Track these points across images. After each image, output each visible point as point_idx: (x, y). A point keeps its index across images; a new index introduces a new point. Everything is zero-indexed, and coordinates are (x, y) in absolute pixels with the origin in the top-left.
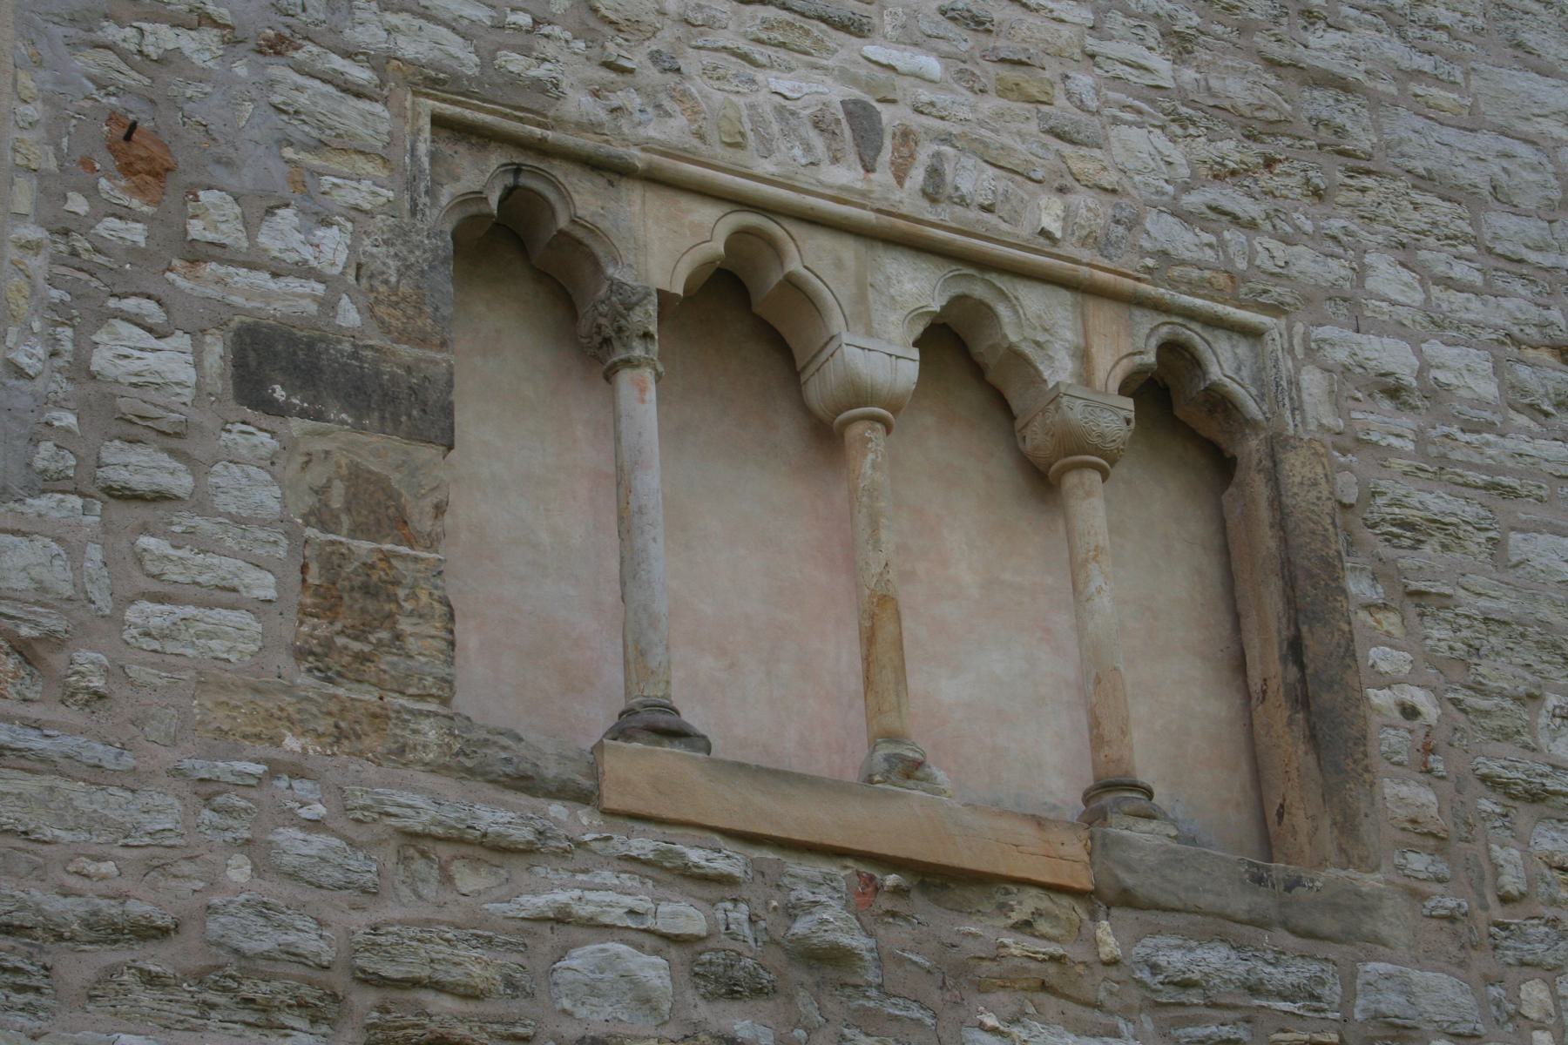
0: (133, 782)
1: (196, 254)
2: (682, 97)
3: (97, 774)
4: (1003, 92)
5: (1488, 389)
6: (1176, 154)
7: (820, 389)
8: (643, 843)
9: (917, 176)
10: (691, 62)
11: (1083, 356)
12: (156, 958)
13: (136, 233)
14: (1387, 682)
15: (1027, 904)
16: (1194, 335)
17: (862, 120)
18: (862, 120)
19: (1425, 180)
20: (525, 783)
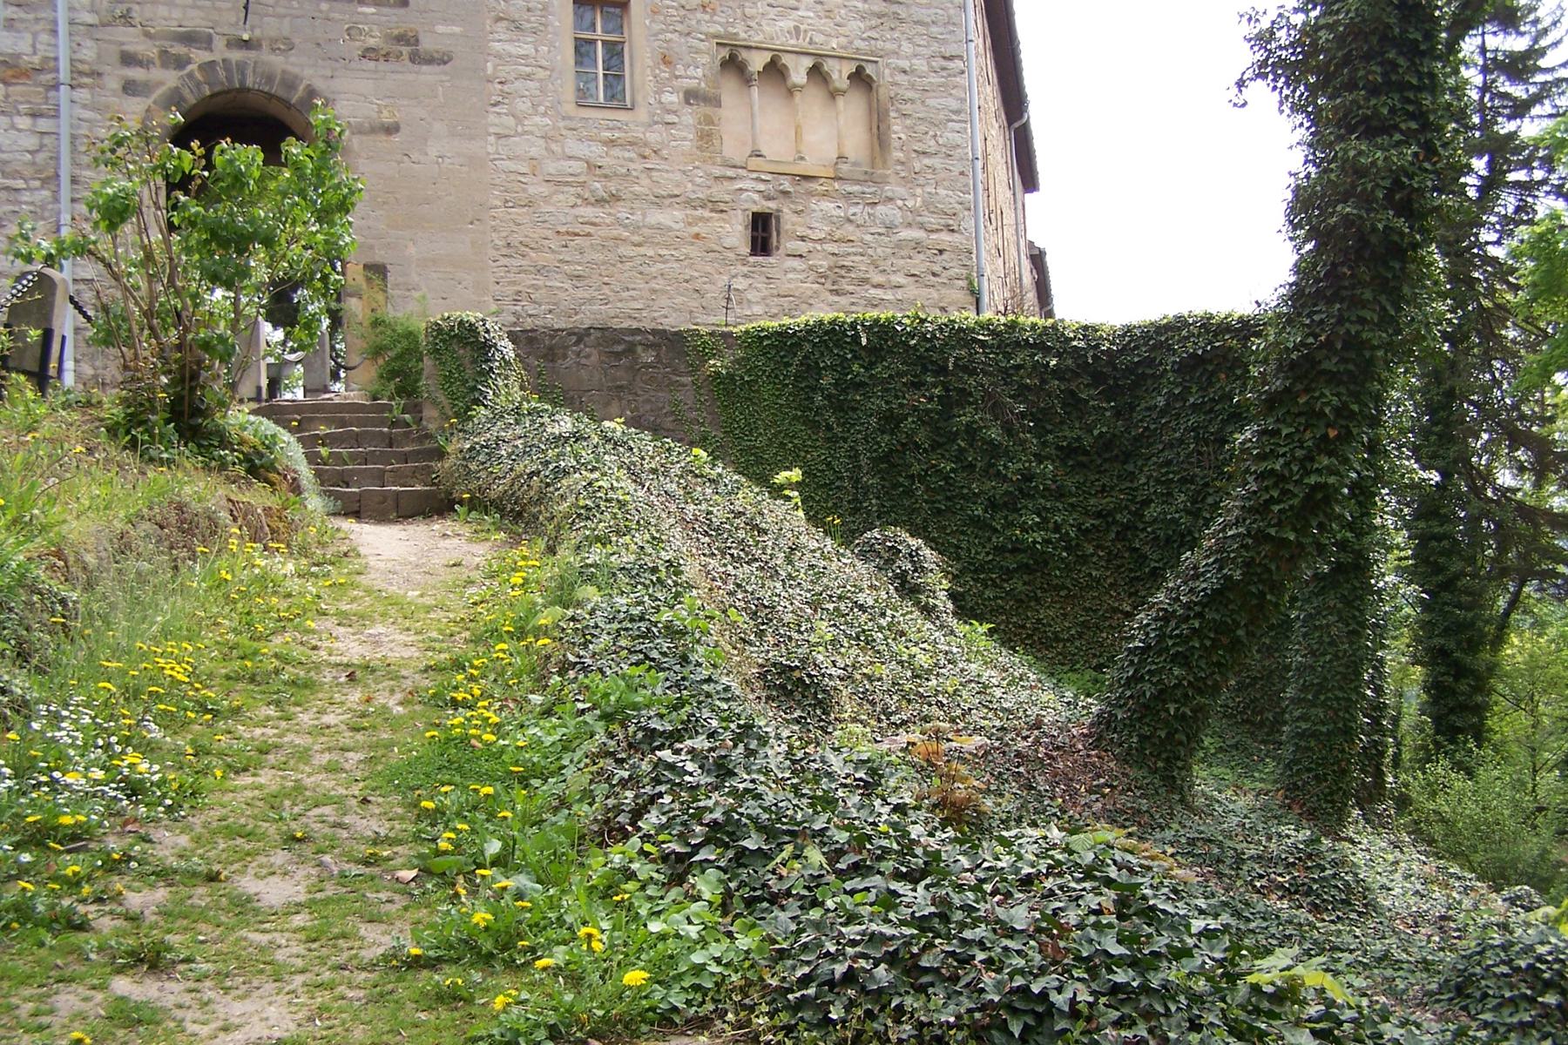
0: (672, 172)
1: (677, 77)
2: (762, 31)
3: (667, 171)
4: (827, 17)
5: (925, 68)
6: (862, 25)
7: (789, 83)
8: (755, 175)
10: (764, 23)
11: (840, 72)
12: (678, 200)
13: (667, 75)
15: (822, 180)
16: (863, 64)
17: (797, 29)
18: (797, 29)
19: (915, 23)
20: (735, 167)
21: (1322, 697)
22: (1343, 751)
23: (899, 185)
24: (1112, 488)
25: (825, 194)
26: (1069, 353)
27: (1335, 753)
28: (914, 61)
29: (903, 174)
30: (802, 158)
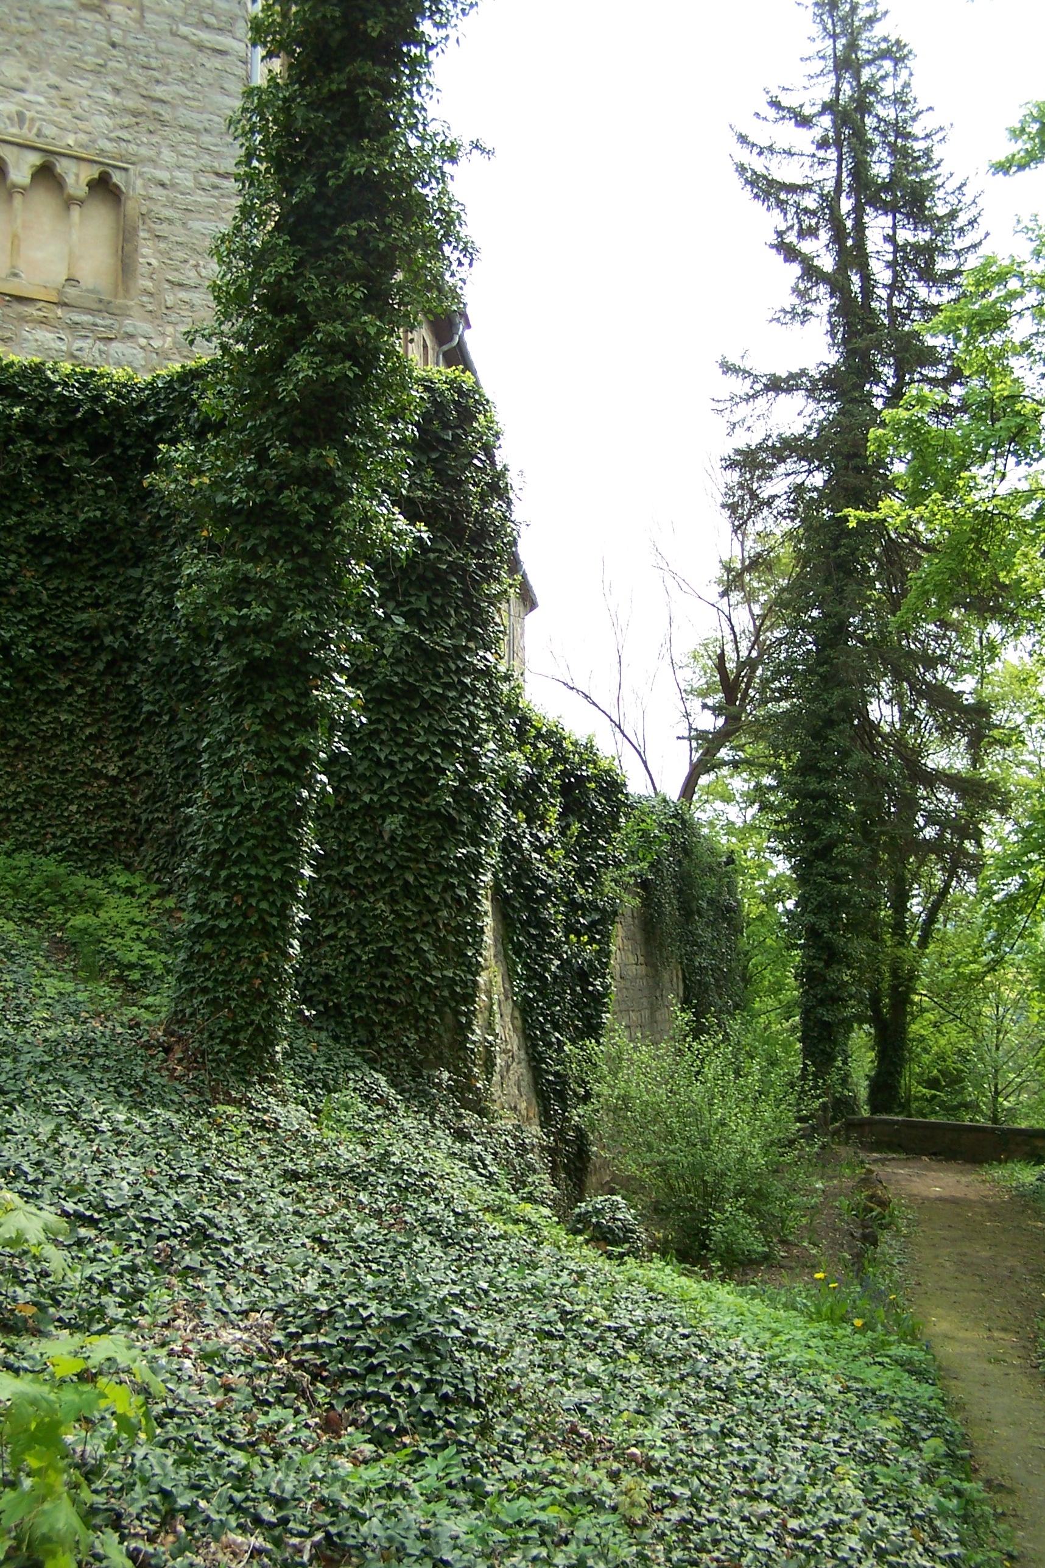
4: (63, 106)
5: (191, 184)
6: (110, 122)
7: (8, 182)
9: (35, 131)
11: (77, 175)
14: (144, 257)
15: (40, 305)
16: (109, 170)
17: (21, 116)
18: (21, 116)
19: (184, 128)
21: (223, 874)
22: (258, 963)
23: (145, 320)
24: (108, 601)
25: (43, 322)
26: (54, 405)
27: (244, 964)
28: (177, 173)
29: (150, 307)
30: (16, 275)
